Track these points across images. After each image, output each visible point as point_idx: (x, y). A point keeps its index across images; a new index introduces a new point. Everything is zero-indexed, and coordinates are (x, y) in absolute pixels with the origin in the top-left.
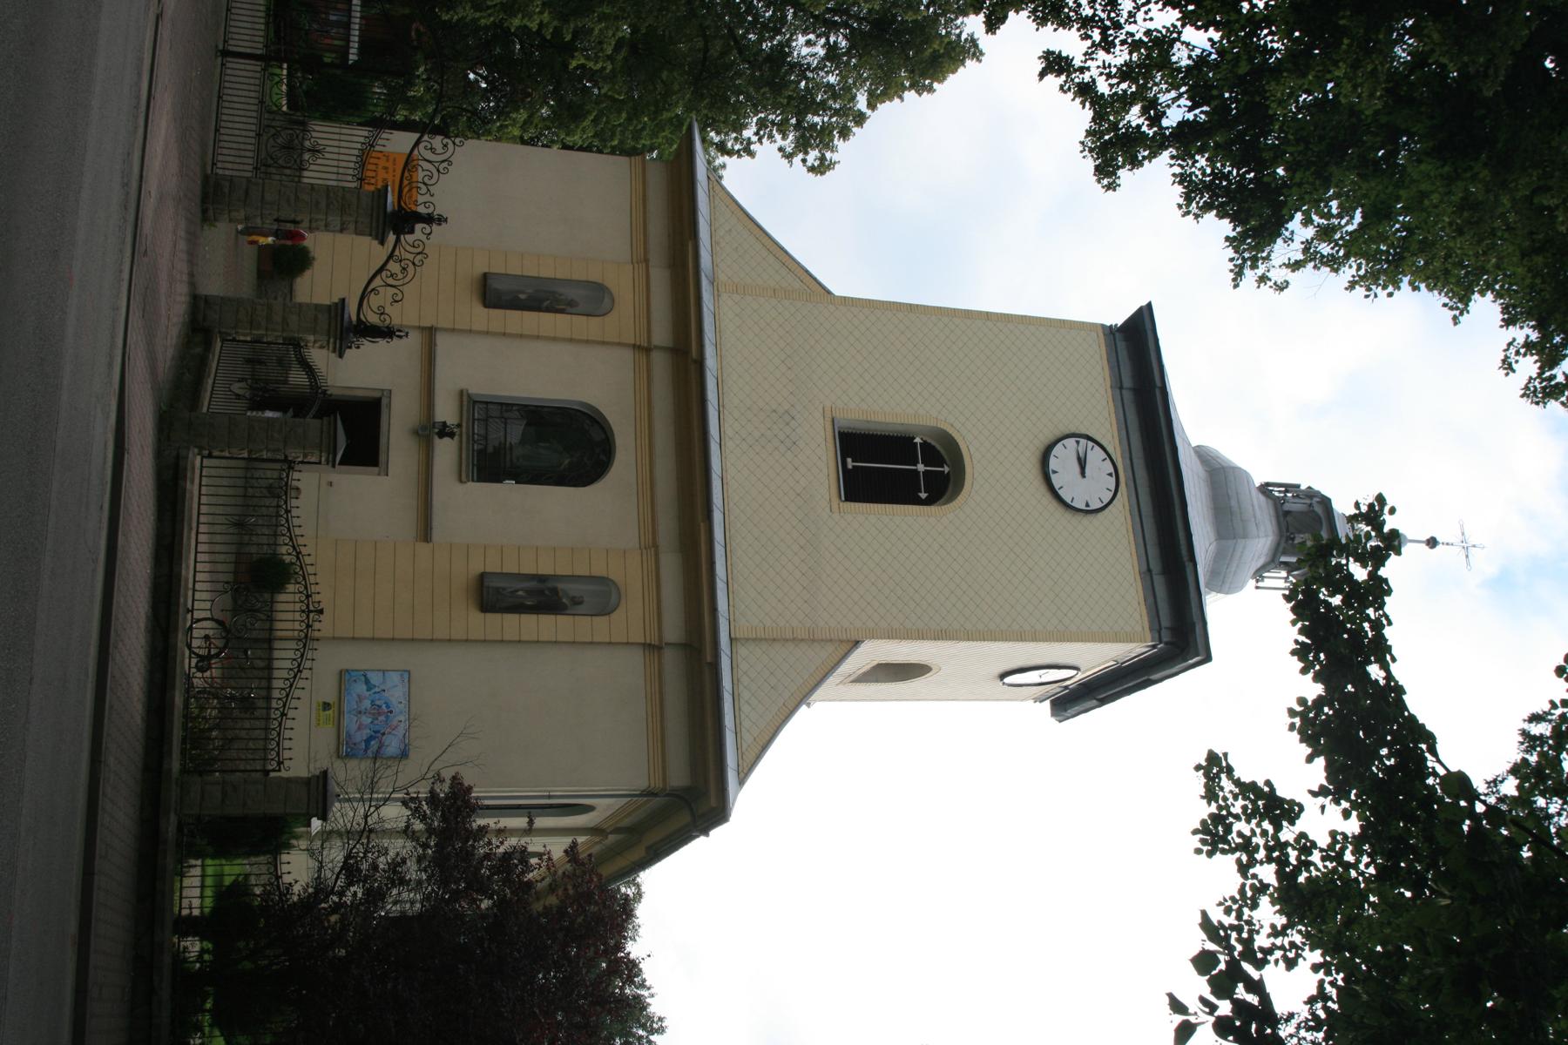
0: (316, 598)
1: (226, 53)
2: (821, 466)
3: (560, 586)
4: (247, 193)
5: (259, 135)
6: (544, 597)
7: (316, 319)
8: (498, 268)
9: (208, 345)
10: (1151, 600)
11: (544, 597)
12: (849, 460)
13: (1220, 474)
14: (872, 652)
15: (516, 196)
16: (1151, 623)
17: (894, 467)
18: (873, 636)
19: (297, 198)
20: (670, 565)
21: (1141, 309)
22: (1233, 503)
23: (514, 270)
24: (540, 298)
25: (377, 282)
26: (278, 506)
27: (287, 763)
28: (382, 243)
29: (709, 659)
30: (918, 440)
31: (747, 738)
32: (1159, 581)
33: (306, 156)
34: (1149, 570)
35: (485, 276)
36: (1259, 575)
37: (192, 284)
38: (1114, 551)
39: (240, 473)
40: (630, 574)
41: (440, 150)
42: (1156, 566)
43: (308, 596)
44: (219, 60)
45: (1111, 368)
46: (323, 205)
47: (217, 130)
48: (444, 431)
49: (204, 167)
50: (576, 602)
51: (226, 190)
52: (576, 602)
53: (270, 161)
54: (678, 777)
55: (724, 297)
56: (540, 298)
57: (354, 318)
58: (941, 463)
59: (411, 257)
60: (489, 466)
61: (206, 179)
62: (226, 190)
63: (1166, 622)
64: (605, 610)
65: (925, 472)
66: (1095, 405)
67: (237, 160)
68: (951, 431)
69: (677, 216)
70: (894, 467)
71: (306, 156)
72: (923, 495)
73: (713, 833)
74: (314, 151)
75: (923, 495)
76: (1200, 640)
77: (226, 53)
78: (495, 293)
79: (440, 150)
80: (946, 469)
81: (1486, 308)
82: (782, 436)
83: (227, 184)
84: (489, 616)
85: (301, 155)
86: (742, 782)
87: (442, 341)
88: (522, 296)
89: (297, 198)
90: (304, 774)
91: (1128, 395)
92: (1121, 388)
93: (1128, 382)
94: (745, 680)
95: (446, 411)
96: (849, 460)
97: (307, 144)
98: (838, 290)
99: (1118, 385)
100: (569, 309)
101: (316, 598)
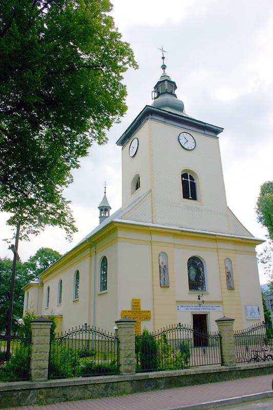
42: (202, 132)
70: (189, 188)
78: (165, 285)
93: (163, 120)
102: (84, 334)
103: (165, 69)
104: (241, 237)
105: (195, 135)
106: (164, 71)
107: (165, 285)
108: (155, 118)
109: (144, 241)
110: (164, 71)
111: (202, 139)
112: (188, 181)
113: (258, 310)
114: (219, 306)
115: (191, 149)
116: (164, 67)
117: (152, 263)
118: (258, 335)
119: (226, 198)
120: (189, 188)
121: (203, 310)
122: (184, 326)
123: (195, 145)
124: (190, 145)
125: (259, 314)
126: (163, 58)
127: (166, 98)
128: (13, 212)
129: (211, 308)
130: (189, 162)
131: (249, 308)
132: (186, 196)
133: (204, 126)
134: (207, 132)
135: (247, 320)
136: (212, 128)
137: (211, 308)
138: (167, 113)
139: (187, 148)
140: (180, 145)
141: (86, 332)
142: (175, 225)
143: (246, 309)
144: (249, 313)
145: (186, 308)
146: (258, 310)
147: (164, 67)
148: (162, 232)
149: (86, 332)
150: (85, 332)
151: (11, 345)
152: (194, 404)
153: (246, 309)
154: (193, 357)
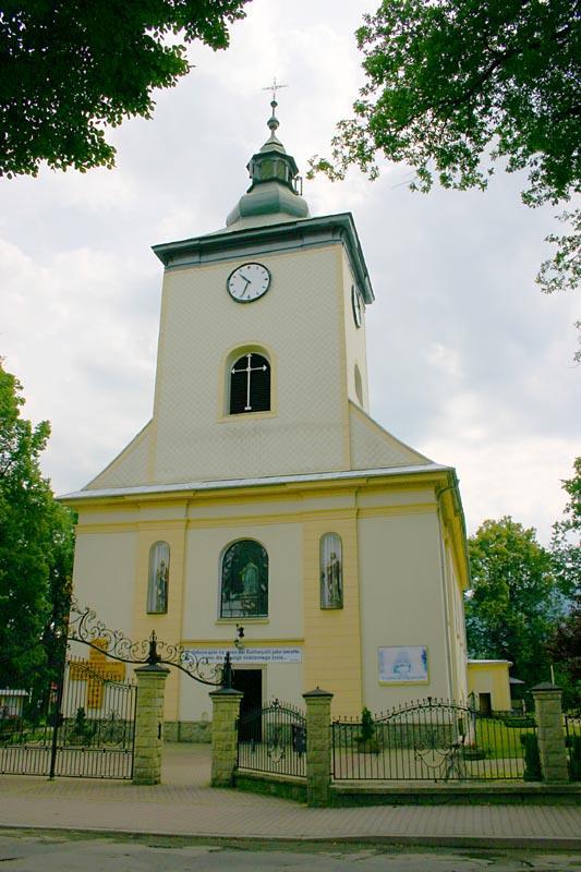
0: (421, 703)
1: (52, 774)
3: (326, 566)
4: (142, 757)
5: (104, 751)
6: (333, 574)
9: (243, 777)
11: (333, 574)
13: (246, 211)
14: (352, 396)
15: (105, 595)
17: (250, 386)
19: (145, 726)
21: (155, 252)
23: (145, 597)
24: (161, 585)
25: (195, 674)
28: (168, 672)
30: (233, 371)
36: (295, 192)
37: (206, 788)
38: (288, 263)
39: (343, 750)
42: (298, 243)
43: (421, 707)
46: (148, 709)
47: (81, 777)
49: (125, 785)
50: (334, 556)
51: (142, 770)
52: (334, 556)
54: (429, 495)
56: (161, 585)
57: (219, 687)
58: (245, 359)
59: (178, 655)
60: (260, 606)
61: (135, 783)
65: (252, 367)
66: (213, 273)
67: (117, 764)
68: (230, 351)
69: (111, 502)
70: (250, 386)
72: (265, 368)
73: (458, 477)
75: (265, 368)
76: (340, 218)
78: (161, 604)
80: (249, 356)
81: (42, 164)
84: (344, 604)
86: (432, 463)
88: (160, 592)
89: (145, 726)
91: (204, 258)
93: (196, 259)
98: (151, 416)
100: (166, 566)
102: (434, 714)
103: (276, 128)
104: (364, 473)
106: (273, 133)
109: (243, 518)
110: (273, 133)
113: (424, 658)
114: (297, 652)
116: (273, 124)
117: (358, 565)
118: (414, 725)
119: (232, 398)
121: (251, 661)
125: (426, 669)
129: (270, 655)
130: (250, 330)
131: (392, 655)
133: (293, 230)
134: (308, 240)
135: (382, 685)
136: (318, 225)
137: (270, 655)
138: (197, 242)
142: (197, 480)
143: (380, 655)
144: (388, 668)
146: (424, 658)
147: (273, 124)
148: (321, 490)
150: (428, 709)
152: (332, 857)
153: (380, 655)
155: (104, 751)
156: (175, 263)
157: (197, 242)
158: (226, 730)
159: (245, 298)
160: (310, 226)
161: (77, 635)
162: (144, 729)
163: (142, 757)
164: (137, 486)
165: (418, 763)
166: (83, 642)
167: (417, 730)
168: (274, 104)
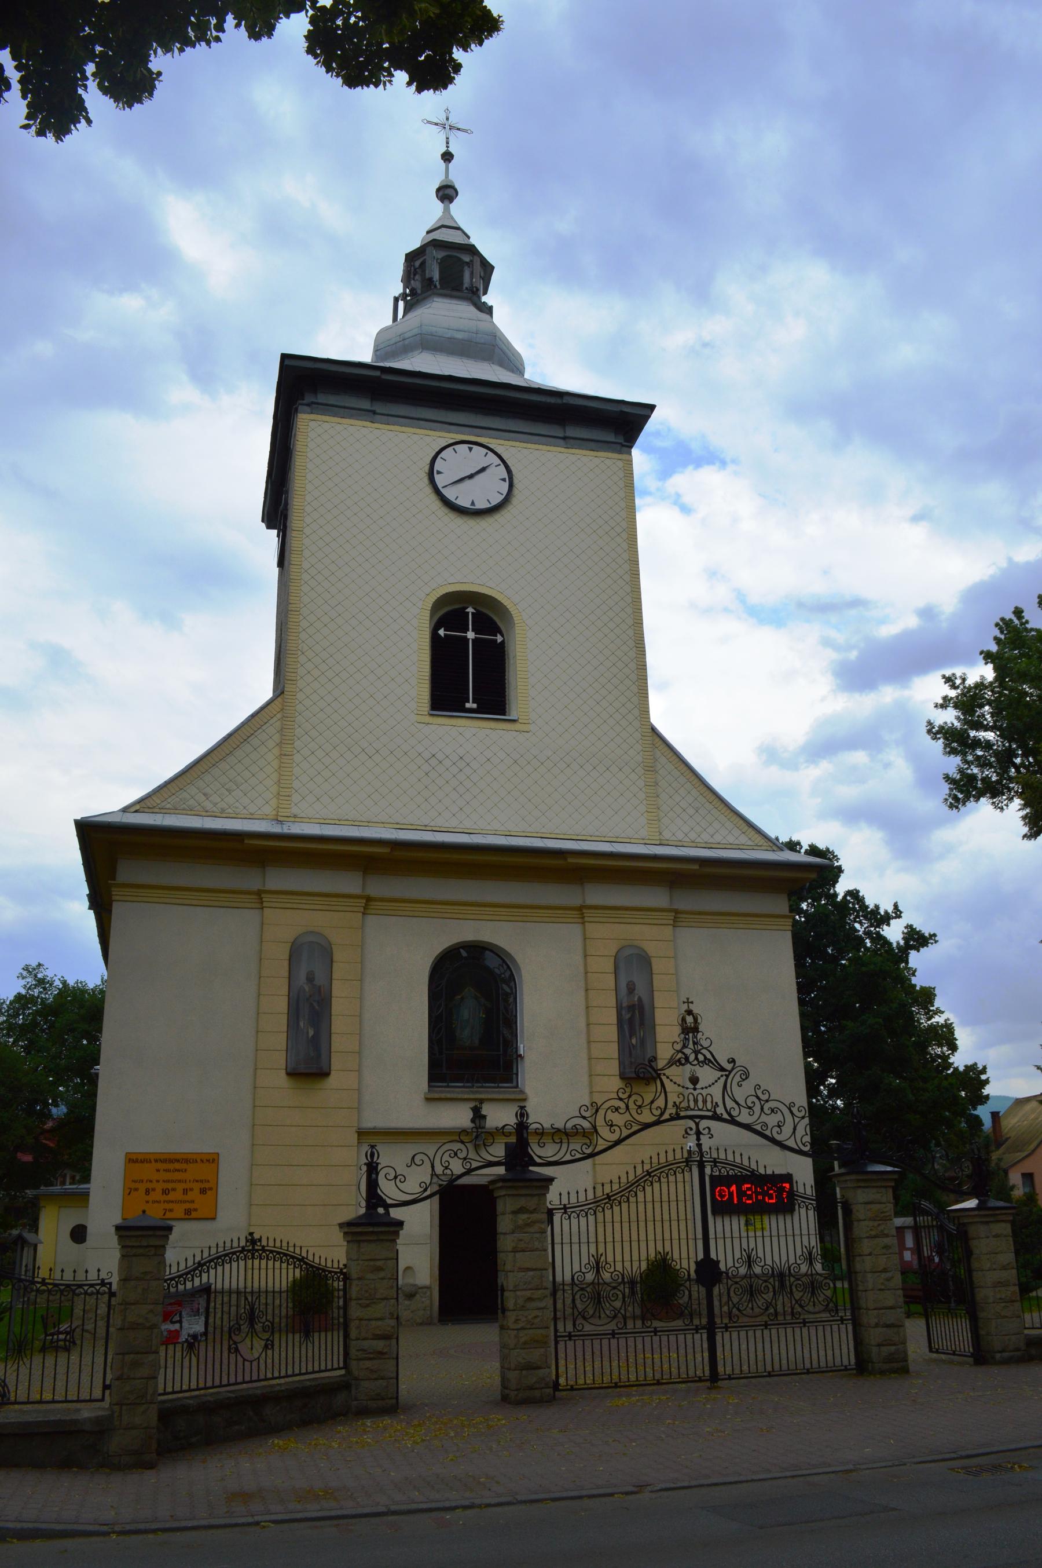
1: (714, 1377)
2: (466, 733)
4: (887, 1326)
7: (996, 1236)
8: (280, 1060)
10: (592, 444)
12: (468, 705)
16: (614, 451)
18: (645, 711)
19: (885, 1270)
20: (598, 895)
22: (459, 336)
23: (280, 1040)
26: (86, 1293)
27: (103, 1275)
28: (551, 1180)
29: (696, 867)
31: (743, 840)
32: (572, 431)
33: (757, 1270)
34: (564, 438)
35: (292, 1074)
40: (609, 936)
41: (778, 1117)
44: (720, 1383)
45: (351, 417)
48: (478, 1116)
53: (772, 1310)
55: (295, 810)
62: (893, 1348)
63: (611, 437)
64: (644, 961)
70: (470, 661)
71: (606, 1276)
72: (442, 632)
74: (750, 1261)
77: (714, 1377)
78: (309, 1067)
79: (778, 1117)
82: (454, 770)
83: (884, 1349)
85: (757, 1276)
87: (372, 1121)
89: (885, 1270)
90: (117, 1254)
91: (379, 407)
92: (374, 413)
93: (366, 404)
94: (693, 836)
95: (458, 1116)
96: (468, 705)
97: (743, 1271)
99: (371, 415)
101: (243, 1243)
105: (509, 448)
106: (447, 210)
107: (309, 1067)
108: (332, 399)
110: (447, 210)
111: (544, 465)
112: (466, 640)
115: (499, 498)
116: (446, 193)
118: (238, 1292)
120: (470, 661)
122: (264, 1243)
123: (511, 486)
124: (485, 491)
126: (447, 157)
127: (444, 313)
128: (1032, 630)
130: (471, 561)
132: (446, 697)
138: (378, 373)
139: (468, 505)
140: (433, 497)
141: (253, 1255)
145: (159, 1165)
147: (446, 193)
149: (253, 1255)
151: (718, 1338)
154: (170, 1371)
155: (655, 1332)
156: (321, 398)
157: (378, 373)
158: (1004, 1268)
159: (450, 494)
160: (586, 407)
161: (720, 1110)
162: (883, 1275)
163: (887, 1326)
164: (251, 817)
165: (232, 1356)
166: (733, 1121)
167: (270, 1298)
168: (447, 157)
